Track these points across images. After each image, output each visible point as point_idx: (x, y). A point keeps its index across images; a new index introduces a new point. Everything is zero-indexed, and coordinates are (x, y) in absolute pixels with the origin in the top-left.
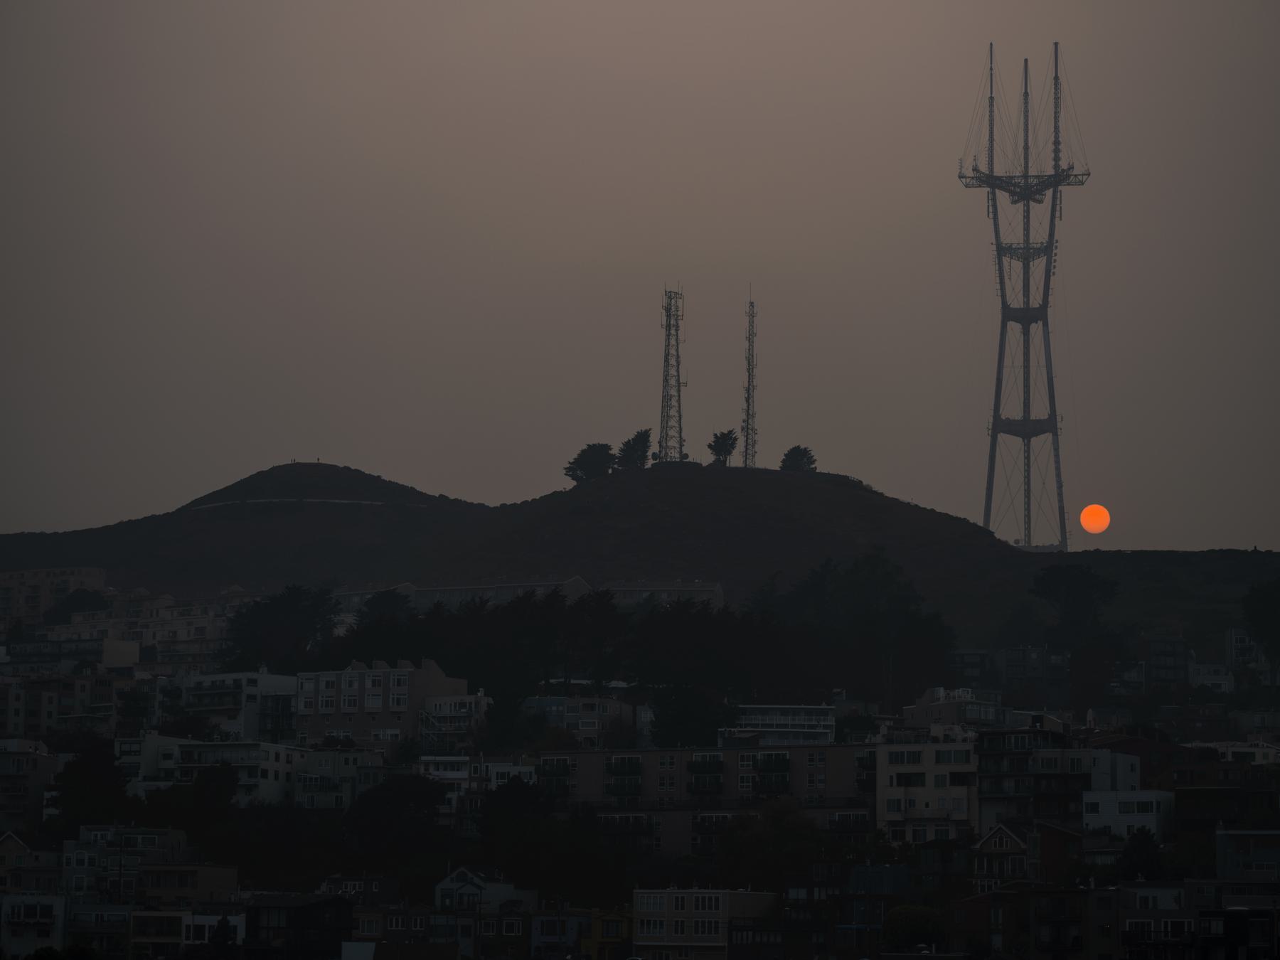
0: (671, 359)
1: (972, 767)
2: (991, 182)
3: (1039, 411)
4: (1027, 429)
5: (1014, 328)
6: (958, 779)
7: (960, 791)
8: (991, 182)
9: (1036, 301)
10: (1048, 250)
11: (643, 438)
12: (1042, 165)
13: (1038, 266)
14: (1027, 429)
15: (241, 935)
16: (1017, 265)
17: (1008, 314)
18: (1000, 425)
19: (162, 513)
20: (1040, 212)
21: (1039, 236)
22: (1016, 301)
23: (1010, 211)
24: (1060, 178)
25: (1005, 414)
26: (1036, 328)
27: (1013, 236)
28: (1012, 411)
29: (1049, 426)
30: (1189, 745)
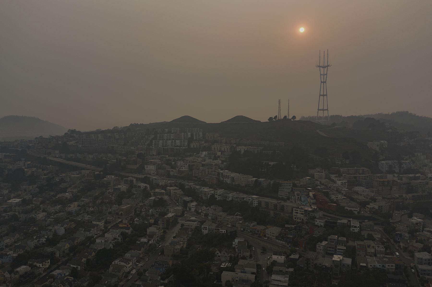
0: (279, 107)
1: (303, 213)
4: (323, 95)
6: (302, 214)
7: (302, 215)
8: (320, 67)
9: (325, 81)
10: (326, 74)
11: (276, 116)
13: (325, 76)
14: (323, 95)
17: (321, 82)
18: (320, 95)
19: (219, 122)
20: (326, 69)
22: (322, 81)
24: (328, 66)
25: (321, 94)
26: (325, 84)
27: (322, 73)
28: (322, 93)
29: (326, 95)
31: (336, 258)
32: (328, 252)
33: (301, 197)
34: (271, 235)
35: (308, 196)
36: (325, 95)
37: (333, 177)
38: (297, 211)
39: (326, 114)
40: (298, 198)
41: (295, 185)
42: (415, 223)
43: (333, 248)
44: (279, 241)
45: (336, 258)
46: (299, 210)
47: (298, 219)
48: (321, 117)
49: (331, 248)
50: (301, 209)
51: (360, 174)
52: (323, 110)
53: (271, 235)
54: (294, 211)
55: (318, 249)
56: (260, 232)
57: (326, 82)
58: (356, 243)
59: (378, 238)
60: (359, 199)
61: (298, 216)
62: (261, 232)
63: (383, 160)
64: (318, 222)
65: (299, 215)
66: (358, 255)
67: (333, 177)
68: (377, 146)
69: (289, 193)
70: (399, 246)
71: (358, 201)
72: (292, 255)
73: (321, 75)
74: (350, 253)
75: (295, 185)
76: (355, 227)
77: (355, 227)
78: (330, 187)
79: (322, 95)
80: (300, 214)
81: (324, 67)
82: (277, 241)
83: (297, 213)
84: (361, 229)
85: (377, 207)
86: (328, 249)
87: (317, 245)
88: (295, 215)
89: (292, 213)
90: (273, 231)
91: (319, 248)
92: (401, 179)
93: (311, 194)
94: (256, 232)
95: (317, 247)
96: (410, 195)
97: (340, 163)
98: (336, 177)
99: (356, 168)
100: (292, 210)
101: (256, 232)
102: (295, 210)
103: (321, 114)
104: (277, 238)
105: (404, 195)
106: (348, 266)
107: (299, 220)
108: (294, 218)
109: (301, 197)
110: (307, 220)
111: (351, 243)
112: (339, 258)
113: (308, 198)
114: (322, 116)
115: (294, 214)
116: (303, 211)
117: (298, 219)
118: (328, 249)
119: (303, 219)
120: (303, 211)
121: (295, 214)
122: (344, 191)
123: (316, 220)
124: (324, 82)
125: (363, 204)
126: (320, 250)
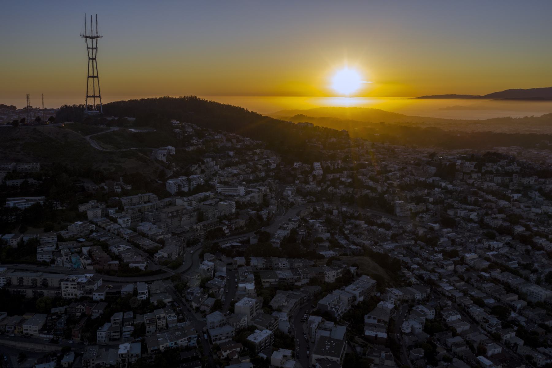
1: (76, 286)
2: (86, 37)
3: (95, 74)
4: (93, 77)
5: (91, 61)
6: (75, 288)
8: (86, 37)
10: (96, 48)
12: (94, 35)
13: (94, 50)
14: (93, 77)
15: (92, 275)
16: (91, 50)
17: (90, 59)
18: (89, 77)
20: (95, 40)
21: (94, 57)
22: (91, 57)
23: (89, 40)
24: (97, 37)
26: (94, 61)
27: (90, 46)
28: (91, 74)
30: (129, 119)
31: (123, 348)
32: (112, 338)
33: (70, 258)
34: (30, 330)
35: (80, 253)
36: (95, 77)
37: (112, 211)
38: (67, 284)
39: (98, 102)
40: (67, 259)
41: (60, 239)
42: (206, 269)
43: (118, 332)
44: (44, 336)
45: (123, 348)
46: (69, 283)
47: (69, 295)
48: (91, 106)
49: (115, 332)
50: (73, 281)
51: (145, 203)
52: (94, 97)
53: (30, 330)
54: (63, 286)
55: (99, 337)
56: (13, 329)
57: (95, 59)
58: (146, 318)
59: (169, 302)
60: (145, 245)
61: (68, 291)
62: (15, 328)
63: (171, 177)
64: (97, 296)
65: (70, 290)
66: (148, 332)
67: (112, 211)
68: (164, 155)
69: (53, 252)
70: (191, 306)
71: (144, 247)
72: (65, 357)
73: (88, 48)
74: (140, 332)
75: (60, 239)
76: (143, 293)
77: (143, 293)
78: (109, 231)
79: (91, 77)
80: (71, 288)
81: (92, 38)
82: (41, 335)
83: (67, 287)
84: (150, 294)
85: (166, 255)
86: (112, 334)
87: (98, 333)
88: (64, 291)
89: (60, 288)
90: (32, 325)
91: (101, 336)
92: (191, 205)
93: (85, 250)
94: (7, 329)
95: (98, 335)
96: (201, 224)
97: (120, 190)
98: (117, 212)
99: (140, 195)
100: (60, 284)
101: (7, 329)
102: (64, 284)
103: (91, 102)
104: (40, 332)
105: (195, 227)
106: (137, 355)
107: (71, 297)
108: (63, 295)
109: (70, 258)
110: (81, 295)
111: (138, 321)
112: (126, 348)
113: (81, 257)
114: (93, 104)
115: (63, 289)
116: (75, 285)
117: (69, 295)
118: (112, 334)
119: (75, 295)
120: (75, 285)
121: (65, 289)
122: (126, 234)
123: (94, 293)
124: (93, 59)
125: (151, 253)
126: (102, 337)
